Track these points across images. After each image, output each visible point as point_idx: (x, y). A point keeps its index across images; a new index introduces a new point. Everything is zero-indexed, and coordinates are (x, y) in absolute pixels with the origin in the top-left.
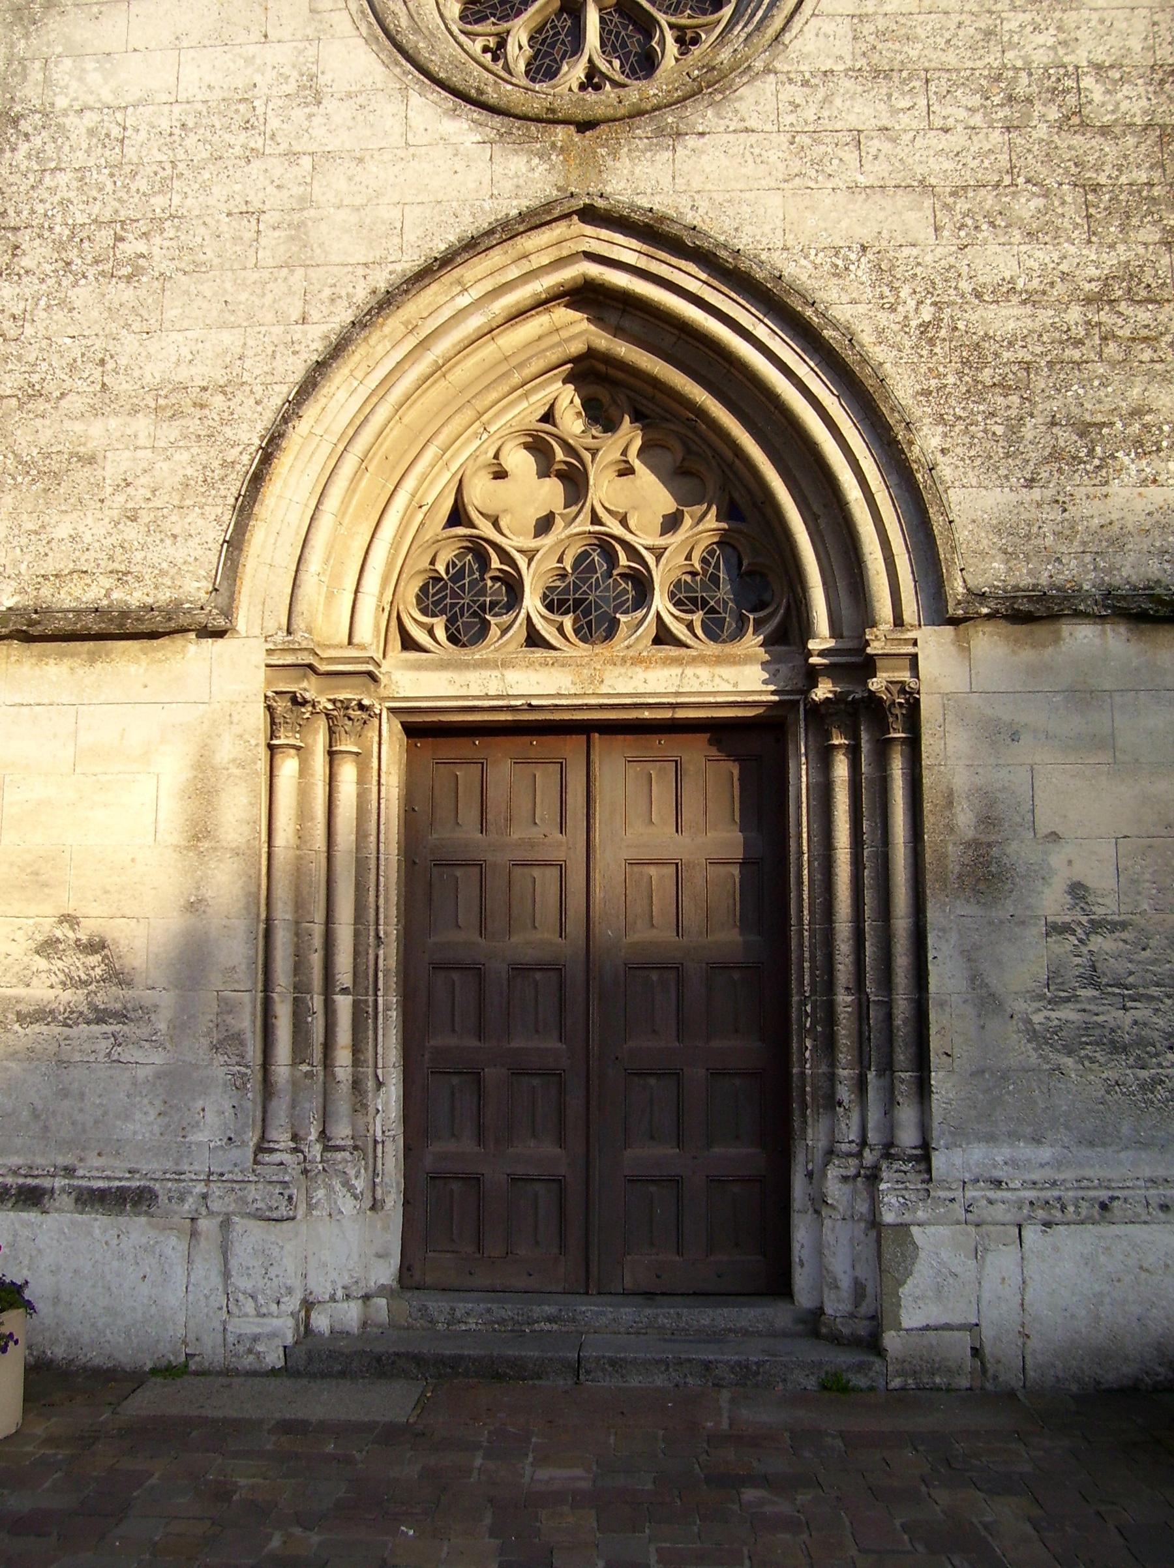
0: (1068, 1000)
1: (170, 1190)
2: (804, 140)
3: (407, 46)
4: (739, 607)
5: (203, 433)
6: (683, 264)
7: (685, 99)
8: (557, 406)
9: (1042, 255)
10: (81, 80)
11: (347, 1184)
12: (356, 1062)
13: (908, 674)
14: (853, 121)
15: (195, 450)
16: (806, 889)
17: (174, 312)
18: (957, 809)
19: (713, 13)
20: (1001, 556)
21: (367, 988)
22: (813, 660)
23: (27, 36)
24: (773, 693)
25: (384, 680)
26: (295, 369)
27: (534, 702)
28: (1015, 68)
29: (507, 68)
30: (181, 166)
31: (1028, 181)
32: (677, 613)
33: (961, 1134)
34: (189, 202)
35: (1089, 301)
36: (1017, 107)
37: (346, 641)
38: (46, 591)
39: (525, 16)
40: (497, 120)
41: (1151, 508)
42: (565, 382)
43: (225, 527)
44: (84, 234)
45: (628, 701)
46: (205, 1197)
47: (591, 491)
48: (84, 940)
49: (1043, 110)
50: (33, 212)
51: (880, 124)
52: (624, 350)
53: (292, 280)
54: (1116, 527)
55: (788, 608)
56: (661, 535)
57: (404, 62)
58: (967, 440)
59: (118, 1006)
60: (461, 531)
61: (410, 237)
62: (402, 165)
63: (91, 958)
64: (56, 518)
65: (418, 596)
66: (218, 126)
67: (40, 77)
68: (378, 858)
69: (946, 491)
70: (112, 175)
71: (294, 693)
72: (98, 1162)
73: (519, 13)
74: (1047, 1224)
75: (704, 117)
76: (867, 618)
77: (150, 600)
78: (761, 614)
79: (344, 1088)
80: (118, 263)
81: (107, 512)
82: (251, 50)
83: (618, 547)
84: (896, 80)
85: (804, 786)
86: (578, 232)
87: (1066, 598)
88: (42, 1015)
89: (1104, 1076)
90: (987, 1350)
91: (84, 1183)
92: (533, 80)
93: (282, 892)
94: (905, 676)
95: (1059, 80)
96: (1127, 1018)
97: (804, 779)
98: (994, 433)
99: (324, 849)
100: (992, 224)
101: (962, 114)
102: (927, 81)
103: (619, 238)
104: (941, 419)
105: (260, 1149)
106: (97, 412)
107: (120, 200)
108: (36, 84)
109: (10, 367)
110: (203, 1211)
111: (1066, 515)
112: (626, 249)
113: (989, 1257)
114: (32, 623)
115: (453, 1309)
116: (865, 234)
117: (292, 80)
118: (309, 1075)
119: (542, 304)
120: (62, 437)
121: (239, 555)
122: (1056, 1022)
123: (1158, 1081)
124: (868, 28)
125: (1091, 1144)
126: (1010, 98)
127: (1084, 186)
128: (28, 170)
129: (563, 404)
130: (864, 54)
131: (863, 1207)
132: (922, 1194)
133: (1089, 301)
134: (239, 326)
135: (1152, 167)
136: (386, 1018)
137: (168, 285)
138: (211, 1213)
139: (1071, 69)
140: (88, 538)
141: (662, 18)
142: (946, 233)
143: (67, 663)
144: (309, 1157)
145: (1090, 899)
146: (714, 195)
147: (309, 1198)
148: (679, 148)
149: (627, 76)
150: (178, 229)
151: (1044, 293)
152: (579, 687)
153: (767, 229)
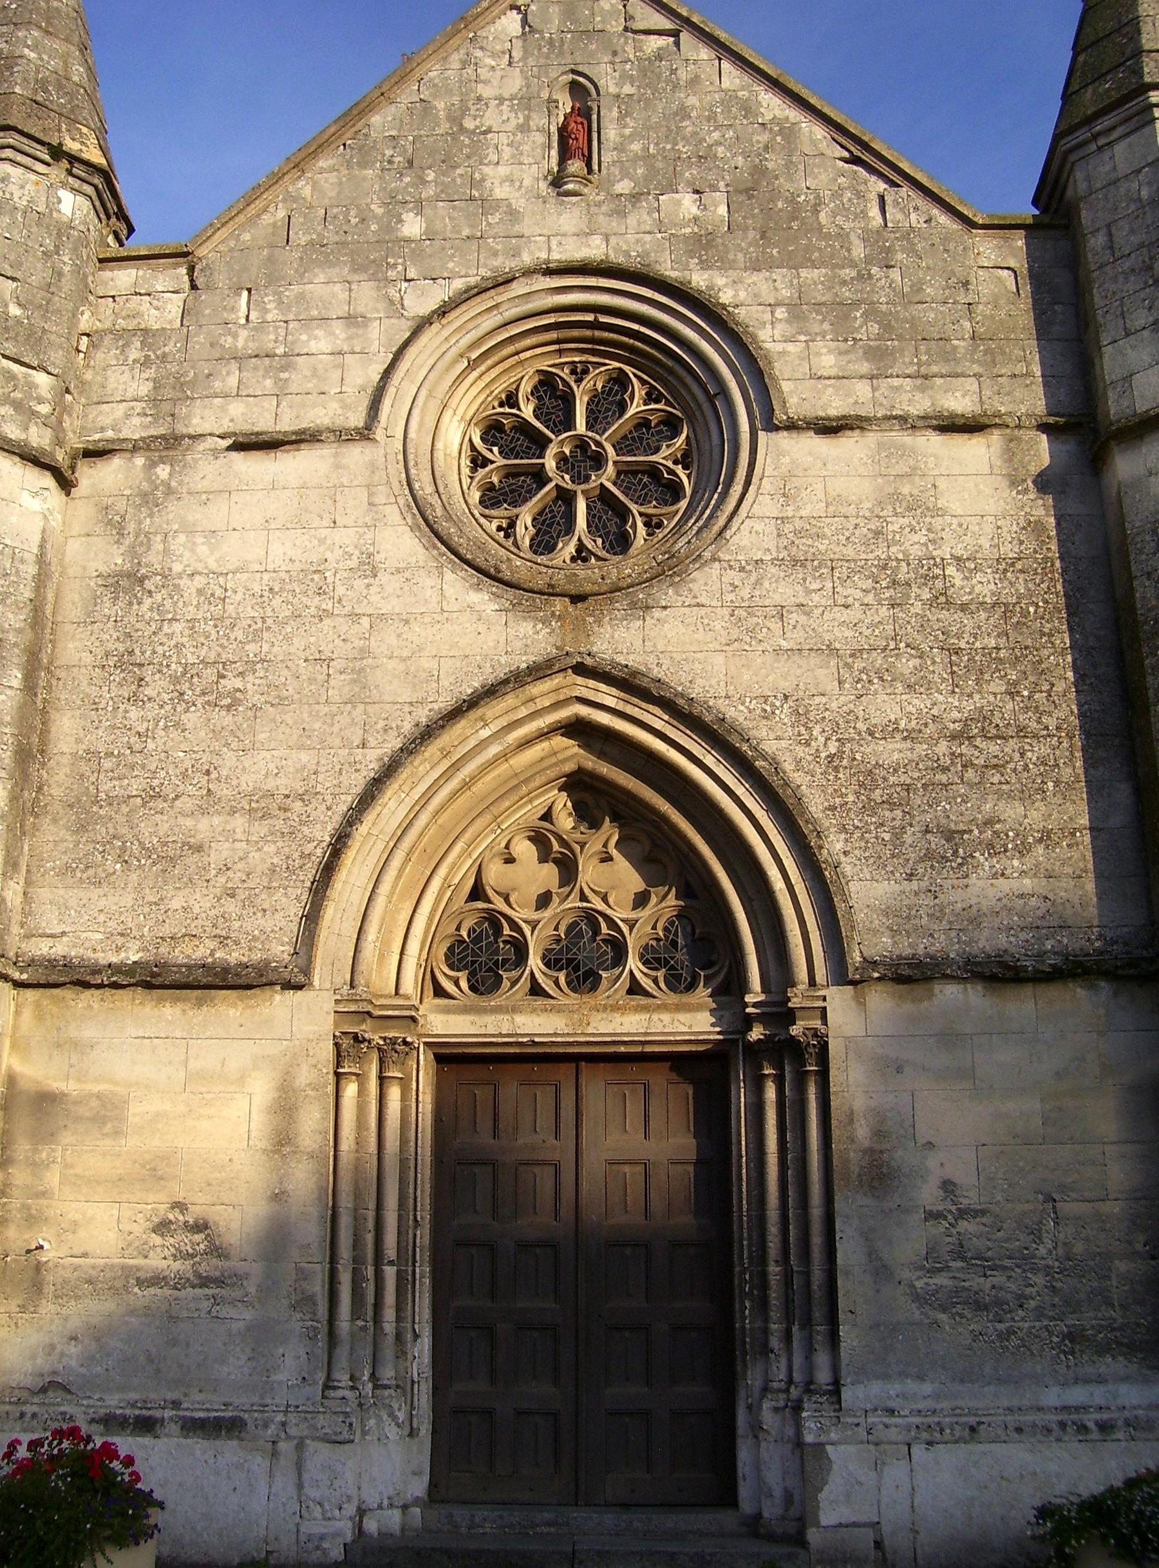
0: (941, 1270)
1: (256, 1420)
2: (742, 613)
3: (443, 533)
4: (693, 964)
5: (286, 831)
6: (651, 707)
7: (652, 579)
8: (554, 808)
9: (919, 703)
10: (193, 551)
11: (392, 1415)
12: (399, 1319)
13: (819, 1022)
14: (777, 599)
15: (280, 844)
16: (744, 1184)
17: (264, 736)
18: (857, 1125)
19: (672, 504)
20: (888, 933)
21: (407, 1260)
22: (749, 1010)
23: (151, 516)
24: (719, 1033)
25: (421, 1021)
26: (357, 783)
27: (537, 1039)
28: (897, 559)
29: (515, 544)
30: (269, 621)
31: (908, 646)
32: (645, 970)
33: (863, 1374)
34: (275, 650)
35: (953, 737)
36: (899, 589)
37: (393, 992)
38: (163, 950)
39: (530, 504)
40: (511, 593)
41: (1000, 895)
42: (560, 790)
43: (303, 904)
44: (194, 672)
45: (609, 1039)
46: (284, 1424)
47: (580, 875)
48: (191, 1221)
49: (918, 591)
50: (154, 652)
51: (798, 601)
52: (605, 769)
53: (355, 713)
54: (974, 909)
55: (730, 967)
56: (633, 909)
57: (439, 545)
58: (863, 844)
59: (218, 1274)
60: (480, 905)
61: (445, 683)
62: (439, 626)
63: (196, 1236)
64: (172, 893)
65: (446, 954)
66: (298, 591)
67: (161, 547)
68: (416, 1159)
69: (847, 884)
70: (216, 626)
71: (356, 1033)
72: (200, 1397)
73: (525, 501)
74: (930, 1443)
75: (666, 594)
76: (789, 981)
77: (245, 960)
78: (710, 972)
79: (390, 1339)
80: (220, 696)
81: (211, 890)
82: (324, 532)
83: (601, 919)
84: (810, 568)
85: (742, 1105)
86: (572, 682)
87: (937, 965)
88: (157, 1280)
89: (971, 1328)
90: (887, 1543)
91: (188, 1414)
92: (535, 552)
93: (345, 1186)
94: (817, 1023)
95: (929, 569)
96: (987, 1284)
97: (742, 1099)
98: (883, 839)
99: (376, 1152)
100: (881, 679)
101: (858, 594)
102: (833, 569)
103: (602, 687)
104: (843, 829)
105: (326, 1387)
106: (204, 812)
107: (221, 646)
108: (158, 553)
109: (136, 773)
110: (283, 1435)
111: (937, 901)
112: (608, 696)
113: (886, 1469)
114: (154, 975)
115: (473, 1516)
116: (786, 686)
117: (354, 557)
118: (364, 1329)
119: (543, 735)
120: (176, 830)
121: (315, 928)
122: (934, 1287)
123: (1010, 1332)
124: (788, 528)
125: (962, 1381)
126: (894, 582)
127: (949, 650)
128: (151, 619)
129: (559, 806)
130: (785, 547)
131: (790, 1431)
132: (834, 1420)
133: (953, 737)
134: (314, 748)
135: (998, 636)
136: (421, 1284)
137: (259, 714)
138: (289, 1437)
139: (938, 560)
140: (196, 910)
141: (634, 508)
142: (847, 686)
143: (180, 1006)
144: (363, 1393)
145: (958, 1193)
146: (674, 655)
147: (363, 1426)
148: (648, 618)
149: (608, 552)
150: (267, 670)
151: (920, 731)
152: (571, 1028)
153: (714, 682)
